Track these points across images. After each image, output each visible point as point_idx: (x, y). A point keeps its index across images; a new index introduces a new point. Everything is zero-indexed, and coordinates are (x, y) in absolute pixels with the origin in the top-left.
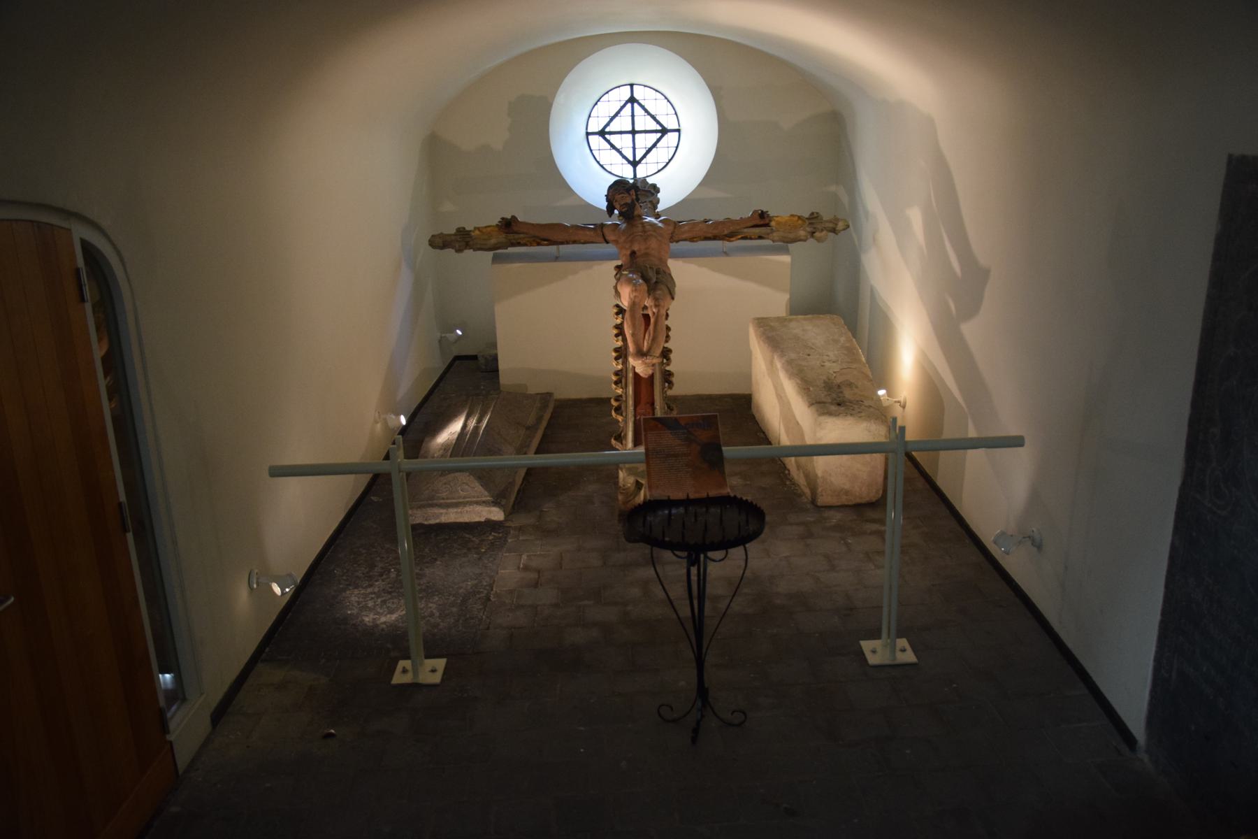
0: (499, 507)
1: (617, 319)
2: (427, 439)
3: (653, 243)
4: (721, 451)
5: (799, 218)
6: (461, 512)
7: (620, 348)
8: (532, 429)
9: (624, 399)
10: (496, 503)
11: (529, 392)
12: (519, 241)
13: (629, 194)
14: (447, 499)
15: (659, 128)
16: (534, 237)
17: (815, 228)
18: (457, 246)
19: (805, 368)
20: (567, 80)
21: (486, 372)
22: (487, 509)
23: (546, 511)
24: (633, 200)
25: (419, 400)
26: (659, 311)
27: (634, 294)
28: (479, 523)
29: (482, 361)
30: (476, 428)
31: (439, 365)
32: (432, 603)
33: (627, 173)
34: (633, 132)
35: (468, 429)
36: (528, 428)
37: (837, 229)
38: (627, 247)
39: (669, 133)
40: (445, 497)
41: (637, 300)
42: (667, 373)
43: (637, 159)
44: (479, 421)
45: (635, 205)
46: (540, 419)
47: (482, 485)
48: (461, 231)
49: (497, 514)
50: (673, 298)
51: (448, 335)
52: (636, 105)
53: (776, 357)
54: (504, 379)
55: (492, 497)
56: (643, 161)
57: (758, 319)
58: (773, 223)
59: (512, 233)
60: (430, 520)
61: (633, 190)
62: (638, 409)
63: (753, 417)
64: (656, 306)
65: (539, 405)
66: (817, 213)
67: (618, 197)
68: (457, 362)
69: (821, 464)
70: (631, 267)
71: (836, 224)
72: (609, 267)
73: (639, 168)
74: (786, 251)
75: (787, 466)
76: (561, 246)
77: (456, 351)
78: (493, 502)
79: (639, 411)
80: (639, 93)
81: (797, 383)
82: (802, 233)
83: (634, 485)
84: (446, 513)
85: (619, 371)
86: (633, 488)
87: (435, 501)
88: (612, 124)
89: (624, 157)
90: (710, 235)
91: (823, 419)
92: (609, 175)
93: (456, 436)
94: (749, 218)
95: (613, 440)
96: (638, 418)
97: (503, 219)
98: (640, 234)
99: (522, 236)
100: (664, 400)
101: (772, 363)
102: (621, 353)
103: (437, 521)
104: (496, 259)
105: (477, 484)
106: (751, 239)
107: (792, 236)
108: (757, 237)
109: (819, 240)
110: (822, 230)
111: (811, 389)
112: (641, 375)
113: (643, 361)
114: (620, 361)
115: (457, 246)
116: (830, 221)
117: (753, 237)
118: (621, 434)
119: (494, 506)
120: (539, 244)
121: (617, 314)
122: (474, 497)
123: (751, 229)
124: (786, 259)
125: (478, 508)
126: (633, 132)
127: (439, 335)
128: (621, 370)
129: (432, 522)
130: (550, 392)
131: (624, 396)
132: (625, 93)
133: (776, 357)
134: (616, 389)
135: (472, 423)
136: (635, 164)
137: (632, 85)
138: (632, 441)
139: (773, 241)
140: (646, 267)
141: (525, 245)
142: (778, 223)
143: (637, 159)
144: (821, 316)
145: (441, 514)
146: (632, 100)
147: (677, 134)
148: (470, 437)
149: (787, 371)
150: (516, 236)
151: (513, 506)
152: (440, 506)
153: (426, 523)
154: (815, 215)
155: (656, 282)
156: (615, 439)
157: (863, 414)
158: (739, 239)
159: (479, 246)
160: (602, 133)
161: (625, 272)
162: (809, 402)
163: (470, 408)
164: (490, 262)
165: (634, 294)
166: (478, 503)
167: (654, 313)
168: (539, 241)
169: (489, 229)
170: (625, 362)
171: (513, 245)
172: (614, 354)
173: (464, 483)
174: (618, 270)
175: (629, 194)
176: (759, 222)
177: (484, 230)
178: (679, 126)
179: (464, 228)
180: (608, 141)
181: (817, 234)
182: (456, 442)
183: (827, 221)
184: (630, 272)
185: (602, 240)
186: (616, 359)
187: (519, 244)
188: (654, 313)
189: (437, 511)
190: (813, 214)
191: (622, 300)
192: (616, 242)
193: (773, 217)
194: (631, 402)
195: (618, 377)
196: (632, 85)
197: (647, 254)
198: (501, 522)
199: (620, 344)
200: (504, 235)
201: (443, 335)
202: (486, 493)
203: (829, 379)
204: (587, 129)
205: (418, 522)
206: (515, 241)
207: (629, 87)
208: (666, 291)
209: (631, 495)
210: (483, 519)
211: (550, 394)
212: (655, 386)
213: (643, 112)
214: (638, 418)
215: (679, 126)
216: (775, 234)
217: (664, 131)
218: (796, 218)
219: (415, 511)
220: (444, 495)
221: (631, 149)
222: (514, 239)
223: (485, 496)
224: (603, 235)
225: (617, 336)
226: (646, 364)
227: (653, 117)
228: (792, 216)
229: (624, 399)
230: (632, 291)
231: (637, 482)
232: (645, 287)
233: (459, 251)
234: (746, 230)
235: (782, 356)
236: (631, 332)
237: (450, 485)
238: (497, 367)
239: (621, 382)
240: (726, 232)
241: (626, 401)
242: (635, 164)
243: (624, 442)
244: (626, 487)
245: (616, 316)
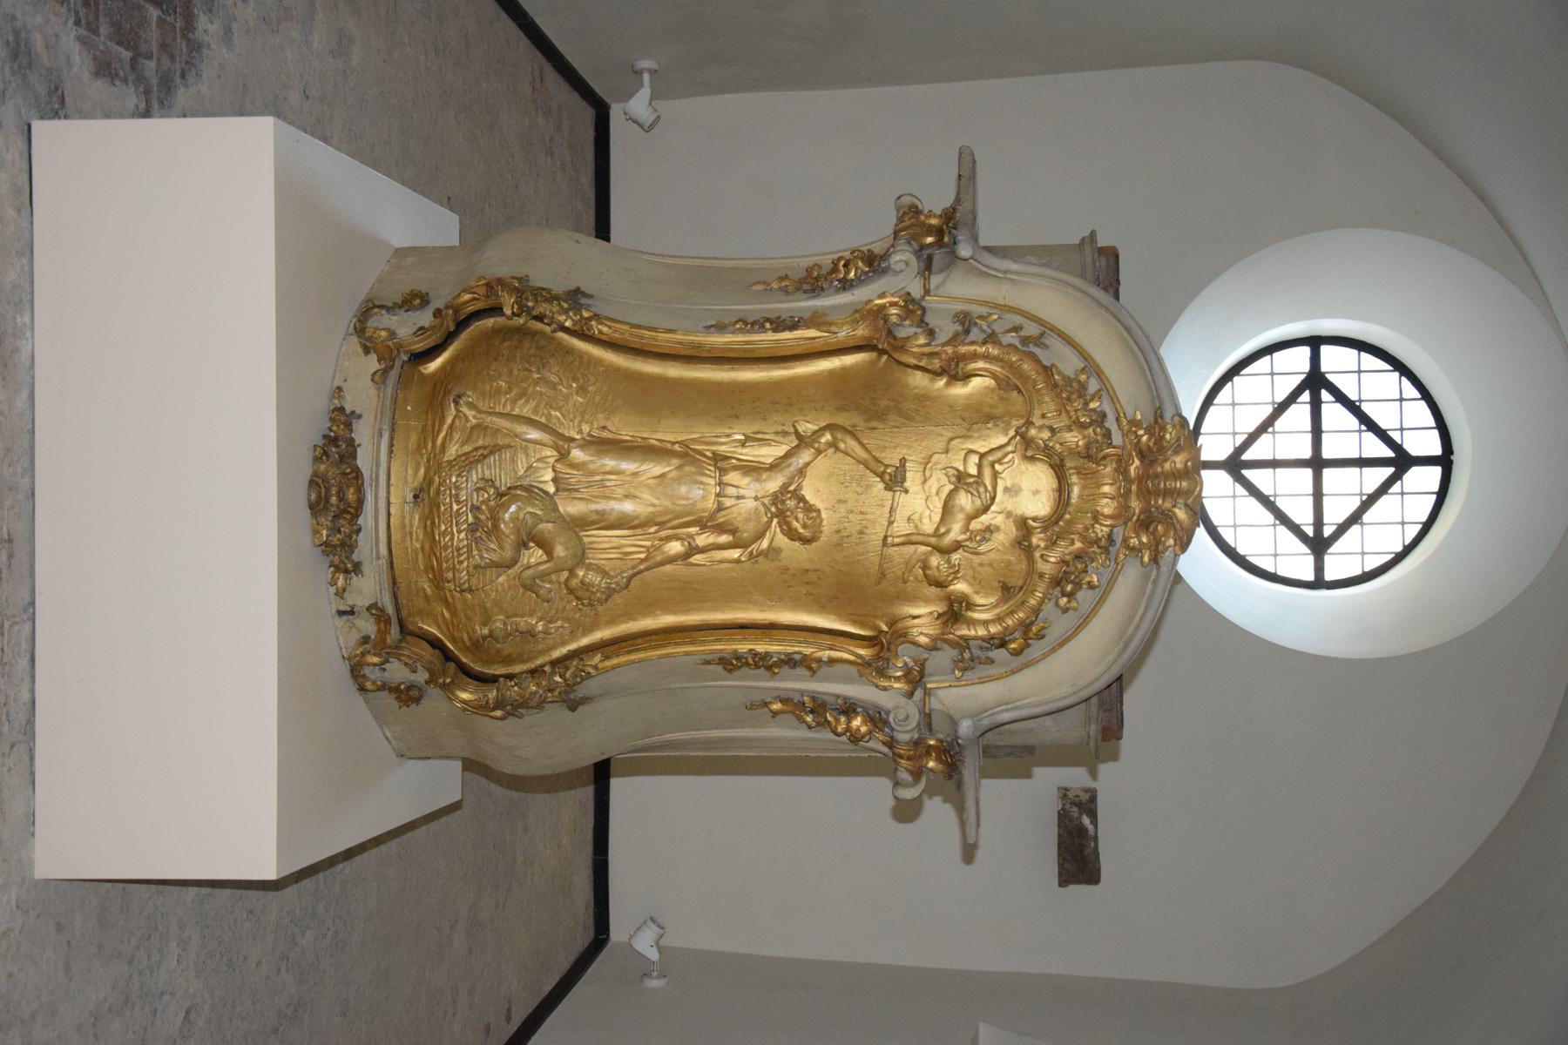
15: (1328, 531)
32: (590, 385)
33: (1214, 446)
34: (1317, 463)
39: (1311, 558)
43: (1248, 473)
52: (1246, 456)
56: (1240, 490)
69: (1035, 262)
88: (1339, 408)
89: (1252, 438)
136: (1234, 465)
143: (1248, 473)
160: (1319, 545)
163: (937, 746)
213: (1265, 439)
221: (1269, 457)
227: (1281, 408)
242: (1234, 465)
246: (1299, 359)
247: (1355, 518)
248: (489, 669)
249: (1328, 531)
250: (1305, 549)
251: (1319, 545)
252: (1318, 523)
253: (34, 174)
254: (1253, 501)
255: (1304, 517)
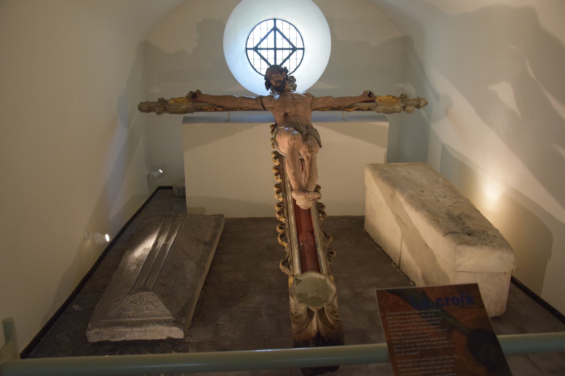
0: (180, 327)
1: (275, 162)
2: (127, 252)
3: (301, 108)
4: (496, 342)
5: (394, 97)
6: (144, 331)
7: (280, 184)
8: (208, 244)
9: (287, 227)
10: (176, 323)
11: (206, 214)
12: (202, 108)
13: (282, 74)
14: (133, 317)
16: (214, 105)
17: (406, 104)
18: (157, 109)
19: (426, 202)
20: (236, 10)
21: (179, 197)
22: (167, 328)
23: (222, 324)
24: (284, 79)
25: (129, 218)
26: (312, 156)
27: (293, 142)
28: (161, 341)
29: (175, 190)
30: (165, 245)
31: (148, 193)
34: (275, 49)
35: (158, 246)
36: (205, 244)
37: (420, 105)
38: (281, 110)
39: (253, 47)
40: (131, 315)
41: (295, 146)
42: (320, 205)
43: (273, 32)
44: (168, 239)
45: (286, 82)
46: (214, 236)
47: (164, 304)
48: (161, 101)
49: (177, 333)
50: (321, 147)
51: (154, 173)
52: (277, 32)
53: (397, 193)
54: (189, 204)
55: (173, 316)
57: (372, 165)
58: (376, 100)
59: (197, 102)
60: (116, 337)
61: (284, 72)
62: (300, 235)
63: (367, 234)
64: (310, 152)
65: (214, 224)
66: (406, 95)
67: (274, 76)
68: (160, 190)
70: (285, 124)
71: (420, 102)
72: (267, 127)
73: (272, 26)
74: (384, 119)
75: (411, 279)
76: (231, 112)
77: (160, 183)
78: (174, 321)
79: (301, 238)
80: (279, 24)
81: (425, 215)
82: (398, 107)
83: (306, 313)
84: (131, 332)
85: (280, 203)
86: (305, 316)
87: (122, 320)
90: (335, 106)
91: (461, 248)
92: (291, 22)
93: (148, 253)
94: (361, 96)
95: (281, 265)
96: (301, 245)
97: (191, 92)
98: (291, 101)
99: (204, 104)
100: (321, 228)
101: (393, 197)
102: (281, 189)
103: (123, 339)
104: (186, 120)
105: (161, 303)
106: (363, 110)
107: (391, 108)
108: (367, 109)
109: (408, 112)
110: (411, 105)
111: (440, 220)
112: (302, 207)
113: (305, 196)
114: (281, 194)
115: (157, 109)
116: (415, 100)
117: (364, 109)
118: (287, 259)
119: (174, 326)
120: (216, 110)
121: (275, 158)
122: (157, 316)
123: (362, 103)
124: (386, 124)
125: (160, 328)
126: (275, 49)
127: (147, 173)
128: (282, 202)
129: (118, 339)
130: (221, 214)
131: (287, 225)
132: (271, 24)
133: (397, 193)
134: (279, 218)
135: (162, 241)
137: (275, 20)
138: (299, 267)
139: (378, 112)
140: (298, 123)
141: (206, 110)
142: (380, 100)
143: (273, 32)
144: (416, 163)
145: (127, 332)
146: (275, 29)
147: (302, 51)
148: (159, 254)
149: (411, 204)
150: (200, 104)
151: (193, 320)
152: (125, 325)
153: (112, 340)
154: (404, 96)
155: (307, 135)
156: (283, 264)
157: (494, 244)
158: (355, 110)
159: (173, 110)
160: (256, 49)
161: (281, 127)
162: (443, 232)
164: (181, 123)
165: (293, 142)
166: (160, 322)
167: (308, 157)
168: (216, 108)
169: (181, 100)
170: (285, 196)
171: (197, 110)
172: (275, 189)
173: (148, 302)
174: (273, 127)
175: (282, 74)
176: (368, 99)
177: (178, 100)
178: (304, 46)
179: (164, 99)
180: (291, 43)
181: (408, 108)
182: (147, 259)
183: (413, 100)
184: (286, 127)
185: (261, 107)
186: (278, 193)
187: (201, 110)
188: (308, 157)
189: (122, 329)
190: (402, 95)
191: (280, 147)
192: (272, 108)
193: (376, 96)
194: (294, 230)
195: (280, 208)
196: (275, 20)
197: (296, 115)
198: (181, 339)
199: (279, 181)
200: (191, 103)
201: (150, 173)
202: (168, 312)
203: (448, 211)
204: (246, 45)
205: (105, 339)
206: (198, 108)
207: (273, 20)
208: (316, 141)
209: (304, 324)
210: (164, 338)
211: (222, 216)
212: (312, 215)
213: (281, 36)
214: (301, 245)
215: (304, 46)
216: (379, 107)
217: (294, 49)
218: (391, 98)
219: (102, 330)
220: (131, 313)
222: (198, 106)
223: (168, 315)
224: (262, 103)
225: (276, 174)
226: (308, 198)
227: (288, 41)
228: (389, 96)
229: (287, 227)
230: (292, 139)
231: (308, 310)
232: (300, 137)
233: (159, 113)
234: (359, 104)
235: (403, 192)
236: (292, 171)
237: (136, 303)
238: (185, 196)
239: (283, 212)
240: (347, 105)
241: (289, 229)
243: (291, 267)
244: (298, 314)
245: (274, 160)
246: (299, 45)
247: (262, 57)
248: (316, 317)
249: (291, 47)
250: (255, 46)
251: (256, 49)
252: (261, 49)
253: (287, 23)
254: (266, 33)
255: (263, 45)
